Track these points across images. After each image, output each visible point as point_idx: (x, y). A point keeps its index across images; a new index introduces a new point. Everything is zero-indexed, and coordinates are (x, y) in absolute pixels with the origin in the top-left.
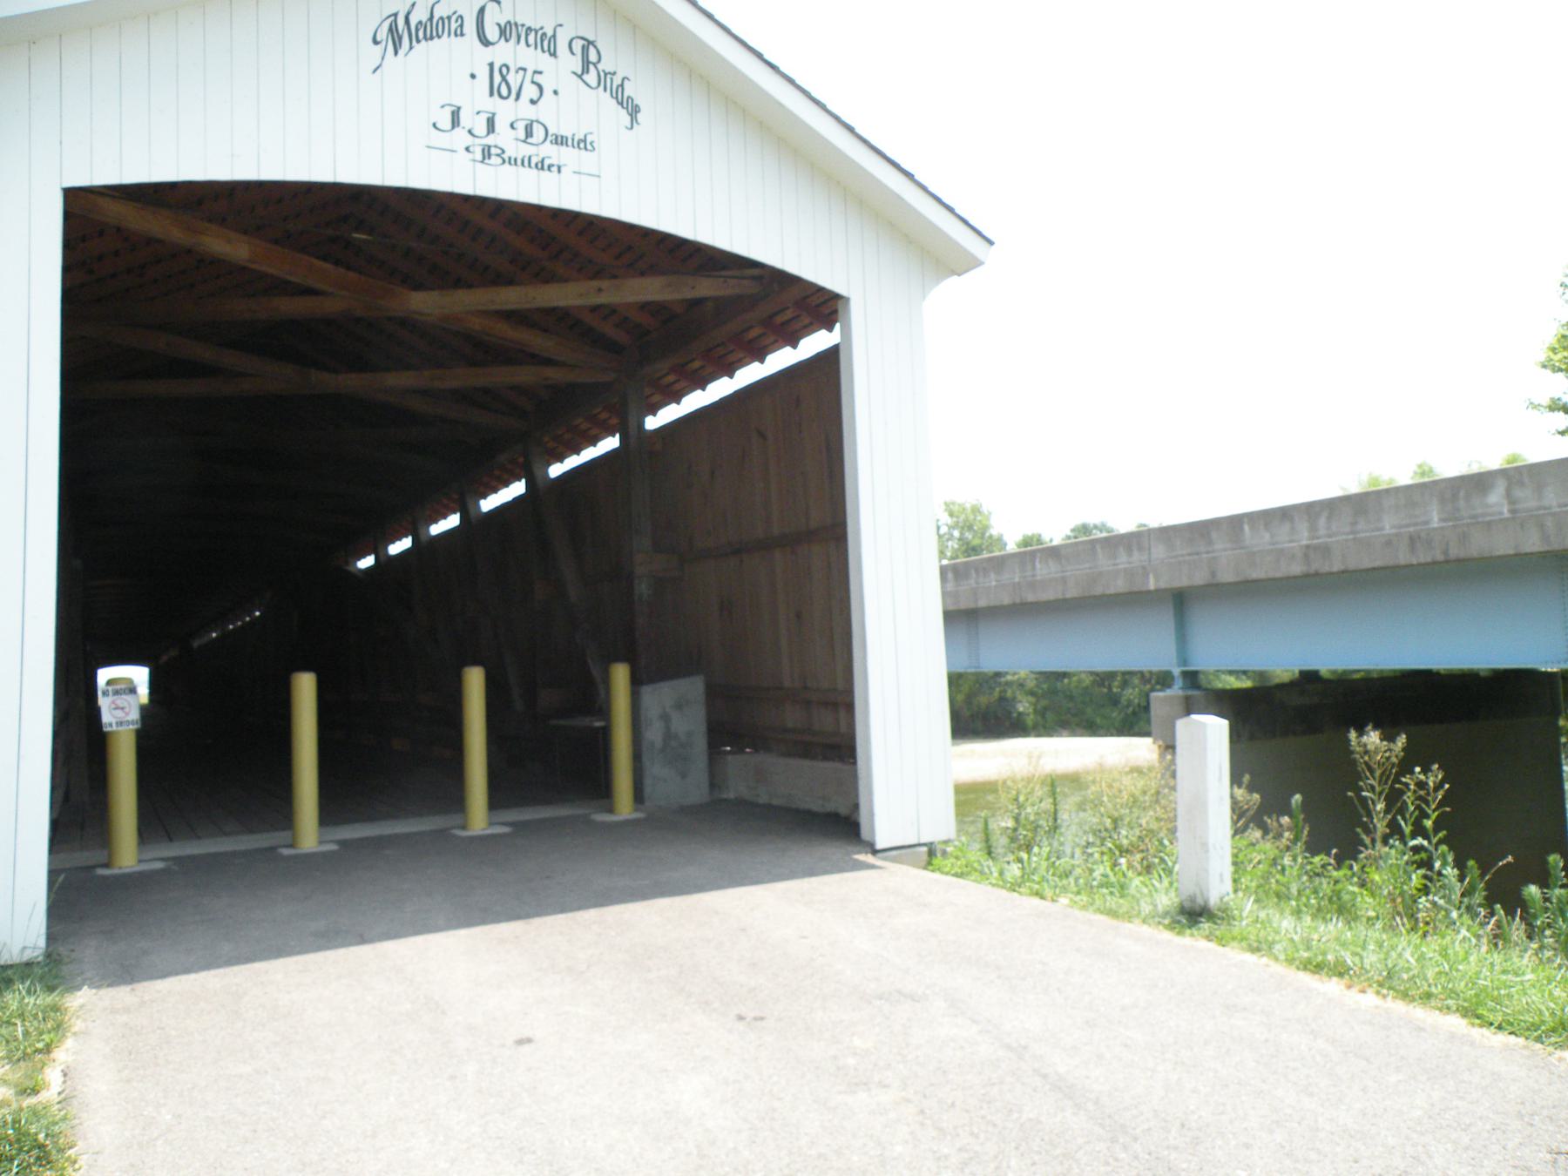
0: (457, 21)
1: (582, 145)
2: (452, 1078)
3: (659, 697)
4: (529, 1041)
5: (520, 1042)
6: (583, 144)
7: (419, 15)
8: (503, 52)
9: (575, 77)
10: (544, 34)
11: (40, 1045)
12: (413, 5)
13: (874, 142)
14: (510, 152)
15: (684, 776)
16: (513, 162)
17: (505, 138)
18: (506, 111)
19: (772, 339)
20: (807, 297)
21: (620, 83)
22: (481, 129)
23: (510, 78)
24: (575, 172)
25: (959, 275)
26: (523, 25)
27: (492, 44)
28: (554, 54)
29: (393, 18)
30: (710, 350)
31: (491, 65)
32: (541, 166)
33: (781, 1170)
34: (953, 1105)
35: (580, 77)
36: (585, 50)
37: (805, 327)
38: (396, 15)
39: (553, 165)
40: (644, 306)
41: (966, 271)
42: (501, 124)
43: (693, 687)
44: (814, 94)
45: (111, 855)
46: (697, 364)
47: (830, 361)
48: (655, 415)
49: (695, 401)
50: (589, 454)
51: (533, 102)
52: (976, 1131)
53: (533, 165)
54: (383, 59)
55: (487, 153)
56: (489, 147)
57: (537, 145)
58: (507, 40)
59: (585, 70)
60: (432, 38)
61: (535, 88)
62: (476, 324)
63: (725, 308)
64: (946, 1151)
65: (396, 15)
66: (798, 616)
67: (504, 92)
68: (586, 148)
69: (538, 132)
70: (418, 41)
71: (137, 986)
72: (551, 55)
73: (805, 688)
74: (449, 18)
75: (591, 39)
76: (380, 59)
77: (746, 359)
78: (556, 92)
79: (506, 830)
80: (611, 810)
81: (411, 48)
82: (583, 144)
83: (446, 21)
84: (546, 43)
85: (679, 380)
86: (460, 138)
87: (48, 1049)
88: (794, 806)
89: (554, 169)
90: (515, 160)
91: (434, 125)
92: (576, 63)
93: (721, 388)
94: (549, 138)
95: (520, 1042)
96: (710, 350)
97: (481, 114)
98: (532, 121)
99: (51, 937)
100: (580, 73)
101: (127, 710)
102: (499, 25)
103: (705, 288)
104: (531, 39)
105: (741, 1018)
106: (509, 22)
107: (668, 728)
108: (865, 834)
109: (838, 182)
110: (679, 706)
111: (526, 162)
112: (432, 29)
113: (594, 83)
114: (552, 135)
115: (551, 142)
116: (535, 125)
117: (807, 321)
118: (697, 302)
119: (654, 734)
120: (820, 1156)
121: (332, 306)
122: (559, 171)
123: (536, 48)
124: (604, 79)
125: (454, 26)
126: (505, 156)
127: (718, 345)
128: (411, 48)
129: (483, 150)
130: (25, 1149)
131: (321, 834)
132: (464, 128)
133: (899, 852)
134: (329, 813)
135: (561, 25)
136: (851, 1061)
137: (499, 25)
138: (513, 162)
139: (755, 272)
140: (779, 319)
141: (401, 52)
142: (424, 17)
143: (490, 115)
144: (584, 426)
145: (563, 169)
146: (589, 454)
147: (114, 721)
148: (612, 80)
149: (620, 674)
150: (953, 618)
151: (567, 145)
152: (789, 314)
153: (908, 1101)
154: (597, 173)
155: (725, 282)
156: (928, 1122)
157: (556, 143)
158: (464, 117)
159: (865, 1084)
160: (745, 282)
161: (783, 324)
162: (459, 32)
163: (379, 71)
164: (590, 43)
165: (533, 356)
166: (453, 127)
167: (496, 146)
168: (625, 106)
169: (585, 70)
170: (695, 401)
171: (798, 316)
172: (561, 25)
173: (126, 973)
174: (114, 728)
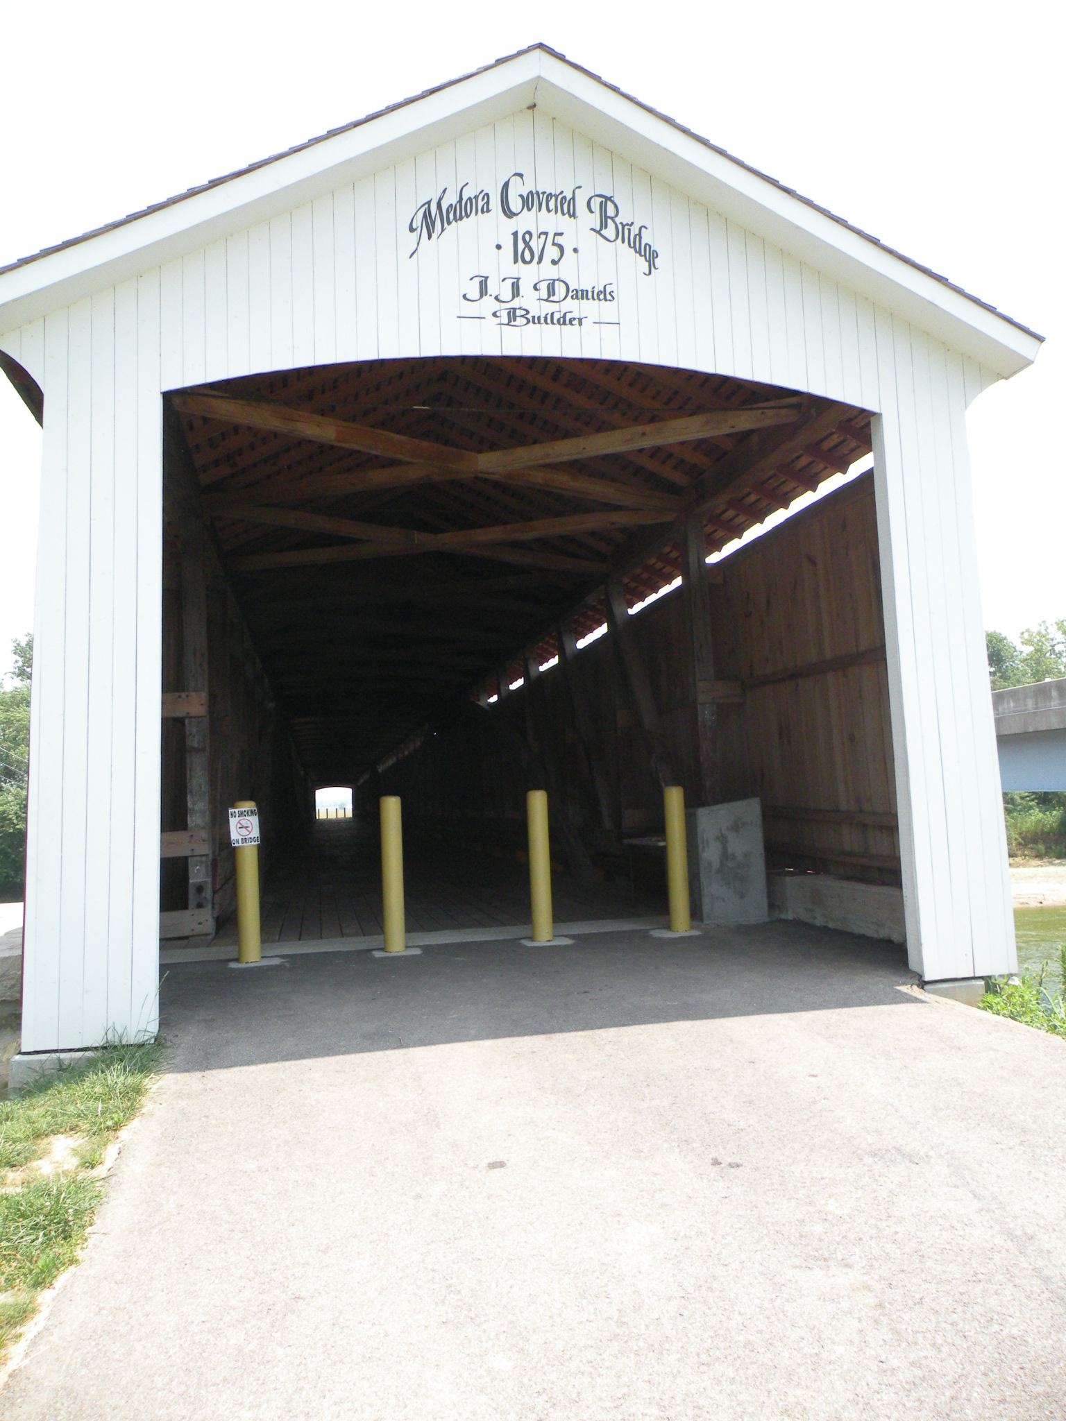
0: (483, 199)
1: (602, 297)
2: (418, 1196)
3: (713, 819)
4: (501, 1165)
5: (493, 1166)
6: (603, 295)
7: (450, 199)
8: (527, 221)
9: (594, 233)
10: (565, 198)
11: (110, 1123)
12: (444, 191)
13: (901, 251)
14: (534, 312)
15: (742, 896)
16: (536, 321)
17: (530, 301)
18: (529, 274)
19: (821, 466)
21: (637, 232)
22: (506, 294)
23: (533, 244)
24: (484, 318)
25: (1007, 379)
26: (544, 193)
27: (516, 215)
28: (573, 215)
29: (427, 206)
30: (763, 483)
31: (515, 234)
32: (563, 321)
33: (698, 1355)
34: (921, 1301)
35: (599, 232)
36: (603, 207)
37: (852, 450)
38: (429, 203)
39: (574, 319)
40: (699, 445)
41: (1015, 373)
42: (526, 287)
43: (750, 809)
44: (834, 212)
45: (240, 951)
46: (753, 498)
47: (867, 479)
48: (720, 551)
49: (754, 532)
50: (665, 590)
51: (554, 262)
52: (939, 1341)
53: (555, 321)
54: (418, 244)
55: (512, 316)
56: (515, 309)
57: (557, 302)
58: (529, 209)
59: (604, 225)
60: (461, 218)
61: (556, 249)
62: (539, 478)
63: (770, 438)
64: (895, 1363)
65: (429, 203)
66: (852, 738)
67: (527, 256)
68: (605, 299)
69: (560, 290)
70: (449, 223)
71: (207, 1073)
72: (570, 216)
73: (861, 811)
74: (476, 197)
75: (609, 196)
76: (416, 245)
77: (799, 489)
78: (575, 250)
79: (569, 942)
80: (668, 927)
81: (443, 230)
82: (603, 295)
83: (474, 201)
84: (565, 207)
85: (738, 515)
86: (488, 304)
87: (116, 1127)
88: (850, 931)
89: (576, 322)
90: (539, 318)
91: (465, 297)
92: (595, 220)
93: (777, 517)
94: (570, 294)
95: (493, 1166)
96: (763, 483)
97: (507, 280)
98: (554, 280)
99: (163, 1023)
100: (598, 229)
101: (250, 829)
102: (521, 196)
103: (744, 421)
104: (552, 204)
105: (716, 1163)
106: (531, 192)
107: (725, 848)
108: (913, 965)
109: (867, 299)
110: (736, 827)
111: (549, 319)
112: (463, 209)
113: (612, 237)
114: (573, 291)
116: (557, 283)
117: (853, 444)
118: (744, 436)
119: (710, 854)
120: (748, 1343)
121: (413, 474)
122: (580, 324)
123: (556, 212)
124: (622, 231)
125: (480, 204)
126: (529, 316)
127: (770, 478)
128: (443, 230)
129: (509, 313)
130: (55, 1221)
131: (407, 940)
132: (491, 295)
133: (949, 985)
134: (414, 922)
135: (580, 187)
136: (819, 1228)
137: (521, 196)
138: (536, 321)
139: (793, 400)
140: (826, 445)
141: (434, 236)
142: (454, 201)
143: (515, 280)
144: (659, 565)
145: (583, 321)
146: (665, 590)
147: (240, 838)
148: (629, 230)
149: (674, 798)
150: (1006, 742)
151: (587, 299)
152: (835, 439)
153: (868, 1288)
154: (617, 322)
156: (885, 1320)
157: (577, 298)
158: (492, 288)
159: (825, 1260)
160: (783, 411)
161: (830, 450)
162: (485, 209)
163: (415, 255)
164: (608, 199)
165: (606, 505)
166: (481, 297)
167: (520, 308)
168: (643, 254)
169: (604, 225)
170: (754, 532)
171: (845, 440)
172: (580, 187)
173: (204, 1061)
174: (240, 844)
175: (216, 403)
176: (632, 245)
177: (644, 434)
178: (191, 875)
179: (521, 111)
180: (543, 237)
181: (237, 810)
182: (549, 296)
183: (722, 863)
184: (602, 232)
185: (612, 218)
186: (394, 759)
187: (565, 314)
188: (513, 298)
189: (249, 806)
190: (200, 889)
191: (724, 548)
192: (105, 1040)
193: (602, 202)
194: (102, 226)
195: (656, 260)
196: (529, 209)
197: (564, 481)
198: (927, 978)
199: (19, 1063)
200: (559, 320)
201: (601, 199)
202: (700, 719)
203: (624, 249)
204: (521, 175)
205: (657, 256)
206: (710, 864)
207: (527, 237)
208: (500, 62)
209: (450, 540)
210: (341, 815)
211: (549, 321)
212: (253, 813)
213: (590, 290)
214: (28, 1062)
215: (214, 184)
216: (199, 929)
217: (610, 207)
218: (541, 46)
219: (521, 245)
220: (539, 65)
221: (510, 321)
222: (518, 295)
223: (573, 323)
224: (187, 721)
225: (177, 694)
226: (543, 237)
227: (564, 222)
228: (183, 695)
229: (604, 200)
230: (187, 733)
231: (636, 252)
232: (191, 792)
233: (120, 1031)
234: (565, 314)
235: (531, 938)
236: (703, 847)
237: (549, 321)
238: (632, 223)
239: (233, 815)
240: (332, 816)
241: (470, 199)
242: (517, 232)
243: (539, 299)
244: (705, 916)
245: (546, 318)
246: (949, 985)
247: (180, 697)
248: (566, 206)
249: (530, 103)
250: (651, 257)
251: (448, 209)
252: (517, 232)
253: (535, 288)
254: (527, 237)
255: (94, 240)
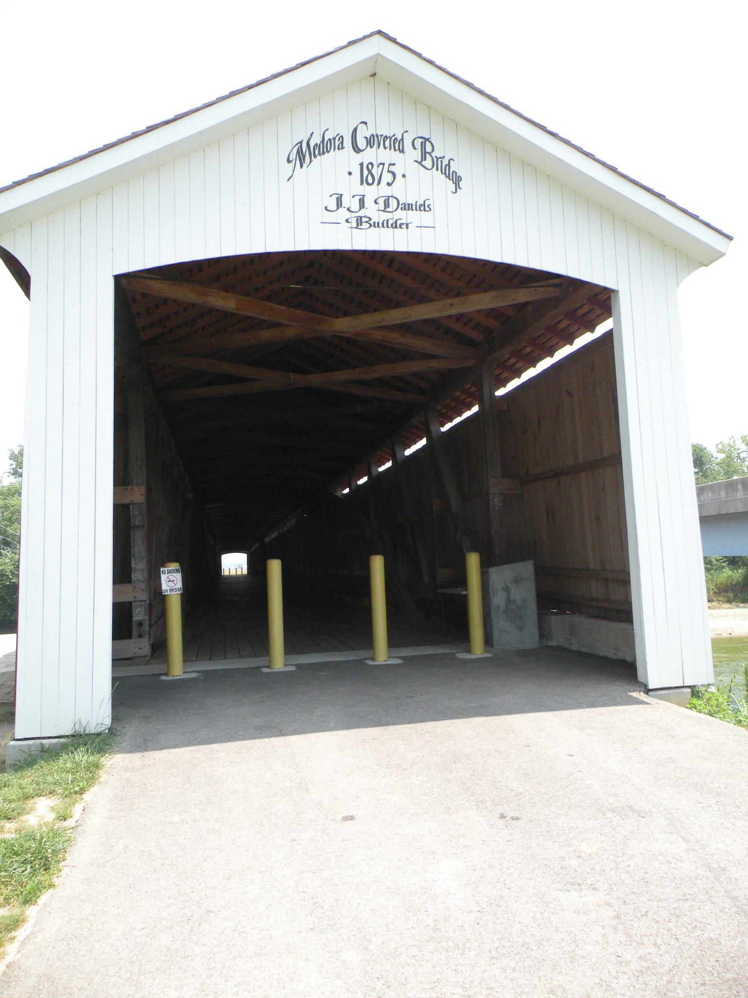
0: (339, 140)
1: (422, 208)
2: (294, 840)
3: (500, 575)
4: (352, 818)
5: (346, 819)
6: (423, 207)
7: (316, 140)
8: (370, 155)
9: (417, 164)
10: (396, 139)
11: (77, 789)
12: (312, 134)
13: (632, 177)
14: (375, 219)
15: (521, 629)
16: (376, 225)
17: (372, 211)
18: (371, 193)
19: (576, 327)
20: (597, 295)
21: (447, 163)
22: (355, 206)
23: (374, 171)
25: (706, 266)
26: (381, 136)
27: (362, 151)
28: (402, 151)
29: (299, 145)
30: (535, 339)
31: (362, 165)
32: (395, 225)
33: (490, 951)
34: (646, 914)
35: (420, 163)
36: (423, 145)
37: (598, 316)
38: (301, 142)
39: (403, 224)
40: (490, 312)
41: (712, 262)
42: (369, 202)
43: (526, 568)
44: (585, 149)
45: (168, 668)
46: (528, 349)
47: (608, 336)
48: (505, 387)
49: (529, 374)
50: (467, 414)
51: (389, 184)
52: (659, 942)
53: (390, 226)
54: (293, 171)
55: (359, 222)
56: (361, 217)
57: (391, 212)
58: (371, 147)
59: (424, 158)
60: (323, 153)
61: (390, 175)
62: (378, 336)
63: (541, 307)
64: (628, 957)
65: (301, 142)
66: (598, 518)
67: (370, 180)
68: (425, 210)
69: (393, 203)
70: (315, 157)
71: (146, 754)
72: (400, 152)
73: (604, 570)
74: (334, 139)
75: (427, 137)
76: (292, 172)
78: (404, 176)
79: (399, 661)
80: (469, 651)
81: (311, 162)
82: (423, 207)
83: (332, 141)
84: (397, 145)
85: (518, 362)
86: (343, 214)
87: (82, 792)
88: (596, 654)
89: (404, 226)
90: (378, 223)
91: (326, 208)
92: (417, 155)
93: (546, 363)
94: (400, 207)
95: (346, 819)
96: (535, 339)
97: (355, 197)
98: (389, 197)
99: (115, 718)
100: (420, 161)
101: (175, 582)
102: (366, 138)
103: (522, 296)
104: (387, 143)
105: (502, 816)
106: (373, 135)
107: (508, 595)
108: (640, 677)
109: (608, 210)
110: (516, 581)
111: (385, 224)
112: (325, 147)
113: (430, 167)
114: (402, 205)
115: (401, 209)
116: (391, 198)
117: (599, 312)
118: (522, 306)
119: (498, 600)
120: (525, 943)
121: (290, 333)
122: (407, 227)
123: (390, 149)
124: (437, 163)
125: (337, 143)
126: (371, 222)
127: (540, 336)
128: (311, 162)
129: (357, 220)
130: (39, 857)
131: (285, 660)
132: (344, 207)
133: (666, 692)
134: (291, 647)
135: (407, 131)
136: (574, 863)
137: (366, 138)
138: (376, 225)
139: (557, 281)
140: (580, 313)
141: (305, 166)
142: (319, 141)
143: (362, 197)
144: (463, 397)
146: (467, 414)
147: (168, 588)
148: (442, 161)
149: (473, 561)
150: (706, 521)
151: (412, 210)
152: (586, 308)
153: (609, 904)
154: (433, 226)
155: (535, 290)
156: (621, 927)
157: (405, 209)
158: (345, 202)
159: (579, 885)
160: (550, 289)
161: (582, 316)
162: (340, 147)
163: (291, 179)
164: (427, 140)
165: (425, 354)
166: (338, 208)
167: (365, 217)
168: (451, 178)
169: (424, 158)
170: (529, 374)
171: (593, 309)
172: (407, 131)
173: (143, 745)
174: (169, 593)
175: (152, 283)
176: (444, 172)
177: (452, 305)
178: (134, 615)
179: (366, 78)
180: (381, 166)
181: (166, 569)
182: (385, 208)
183: (507, 606)
184: (422, 163)
185: (429, 153)
186: (277, 533)
187: (396, 221)
188: (360, 209)
189: (175, 566)
190: (140, 624)
191: (508, 385)
192: (73, 731)
193: (422, 142)
194: (72, 159)
195: (460, 183)
196: (371, 147)
197: (396, 338)
198: (650, 687)
199: (14, 747)
200: (392, 225)
201: (421, 140)
202: (491, 505)
203: (438, 175)
204: (365, 123)
205: (461, 180)
206: (498, 607)
207: (370, 166)
208: (351, 43)
209: (316, 379)
210: (239, 573)
211: (385, 225)
212: (177, 571)
213: (414, 204)
214: (20, 746)
215: (150, 129)
216: (140, 653)
217: (428, 145)
218: (380, 32)
219: (366, 172)
220: (378, 46)
221: (358, 225)
222: (364, 207)
223: (402, 227)
224: (131, 507)
225: (124, 487)
226: (381, 166)
227: (395, 156)
228: (129, 488)
229: (424, 140)
230: (131, 515)
231: (446, 177)
232: (134, 556)
233: (84, 724)
234: (396, 221)
235: (373, 659)
236: (494, 595)
237: (385, 225)
238: (444, 157)
239: (164, 572)
240: (233, 573)
241: (330, 140)
242: (363, 163)
243: (378, 210)
244: (495, 643)
245: (383, 223)
246: (666, 692)
247: (126, 489)
248: (397, 145)
249: (372, 72)
250: (457, 180)
251: (314, 147)
252: (363, 163)
253: (376, 202)
254: (370, 166)
255: (66, 168)
